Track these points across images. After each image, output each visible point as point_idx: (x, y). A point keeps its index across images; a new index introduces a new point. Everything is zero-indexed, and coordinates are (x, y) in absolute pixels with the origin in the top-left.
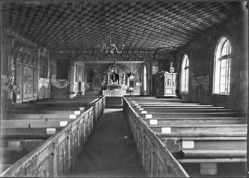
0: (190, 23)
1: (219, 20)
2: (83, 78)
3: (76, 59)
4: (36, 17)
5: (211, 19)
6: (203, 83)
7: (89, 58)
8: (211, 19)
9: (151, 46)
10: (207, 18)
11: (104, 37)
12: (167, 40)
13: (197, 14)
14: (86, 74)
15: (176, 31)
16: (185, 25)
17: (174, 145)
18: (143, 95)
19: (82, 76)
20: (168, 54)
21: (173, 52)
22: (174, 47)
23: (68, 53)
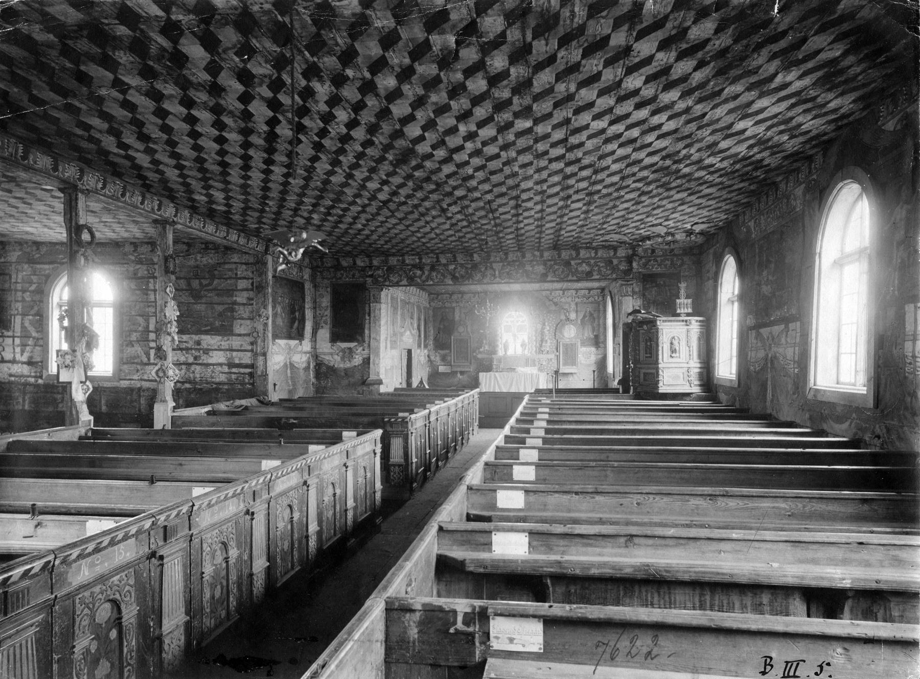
0: (715, 144)
1: (829, 122)
2: (420, 336)
3: (385, 281)
4: (272, 168)
5: (792, 118)
6: (781, 350)
7: (424, 278)
8: (792, 118)
9: (609, 233)
10: (775, 116)
11: (444, 211)
12: (654, 209)
13: (731, 105)
14: (431, 325)
15: (673, 173)
16: (699, 150)
17: (452, 631)
18: (607, 385)
19: (415, 332)
20: (675, 255)
21: (691, 248)
22: (689, 233)
23: (362, 264)
